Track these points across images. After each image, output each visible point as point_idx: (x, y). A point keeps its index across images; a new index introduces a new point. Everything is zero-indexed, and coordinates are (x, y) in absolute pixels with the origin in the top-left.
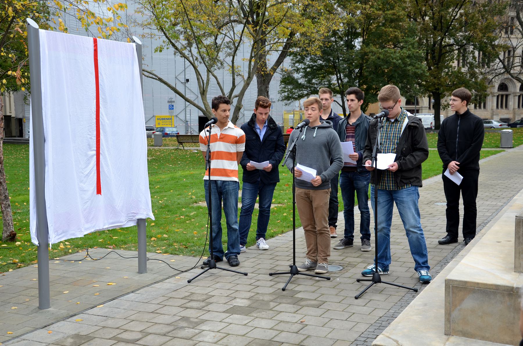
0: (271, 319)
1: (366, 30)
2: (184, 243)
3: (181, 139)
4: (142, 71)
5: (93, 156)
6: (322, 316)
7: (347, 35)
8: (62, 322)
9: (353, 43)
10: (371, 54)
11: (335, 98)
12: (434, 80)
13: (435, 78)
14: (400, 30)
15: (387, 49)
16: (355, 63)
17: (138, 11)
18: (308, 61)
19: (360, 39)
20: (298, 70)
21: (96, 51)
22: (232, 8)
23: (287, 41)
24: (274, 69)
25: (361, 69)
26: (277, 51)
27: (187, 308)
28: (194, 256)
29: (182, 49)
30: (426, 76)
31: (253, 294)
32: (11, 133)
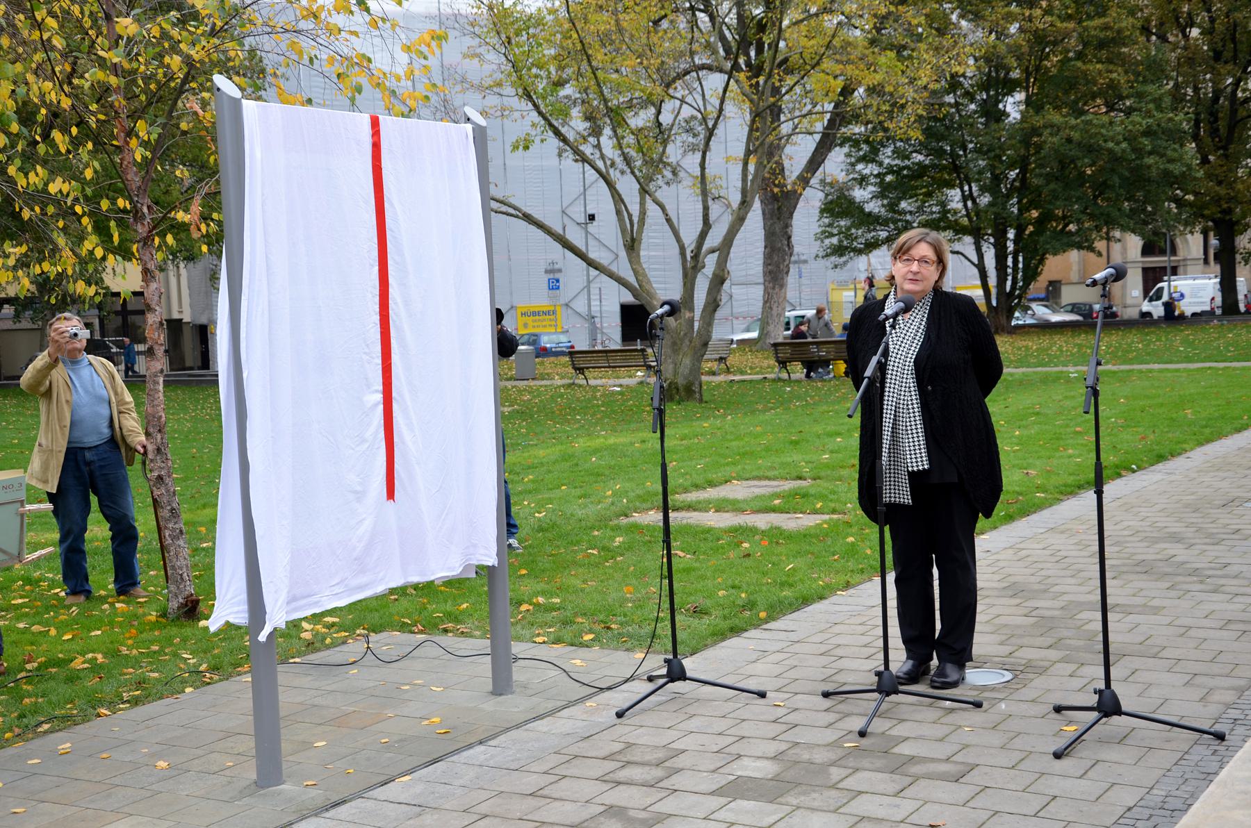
0: (835, 811)
1: (1034, 72)
2: (601, 617)
3: (580, 360)
4: (487, 198)
5: (376, 405)
6: (970, 804)
7: (984, 86)
8: (314, 820)
9: (1001, 106)
10: (1048, 131)
11: (957, 246)
12: (1217, 188)
13: (1220, 183)
14: (1123, 66)
15: (1089, 117)
16: (1008, 157)
17: (472, 55)
18: (887, 156)
19: (1020, 96)
20: (862, 181)
21: (376, 147)
22: (697, 34)
23: (835, 107)
24: (804, 180)
25: (1024, 171)
26: (811, 134)
27: (619, 783)
28: (627, 650)
29: (576, 140)
30: (1195, 179)
31: (784, 747)
32: (182, 359)
